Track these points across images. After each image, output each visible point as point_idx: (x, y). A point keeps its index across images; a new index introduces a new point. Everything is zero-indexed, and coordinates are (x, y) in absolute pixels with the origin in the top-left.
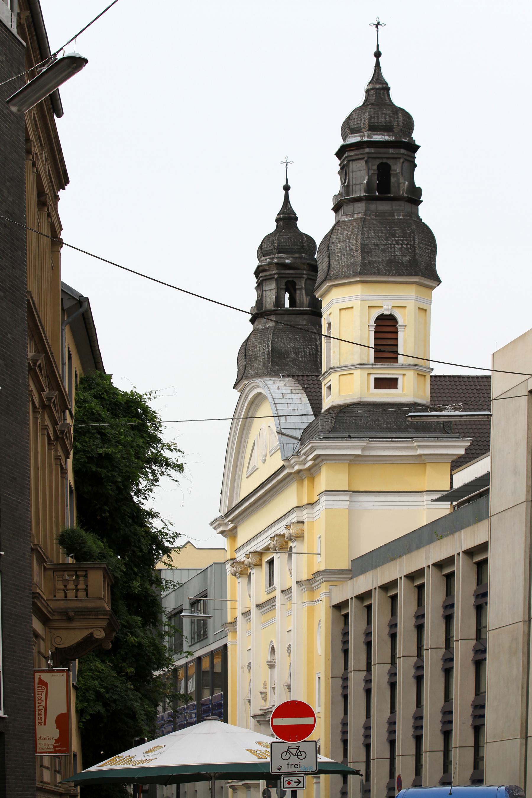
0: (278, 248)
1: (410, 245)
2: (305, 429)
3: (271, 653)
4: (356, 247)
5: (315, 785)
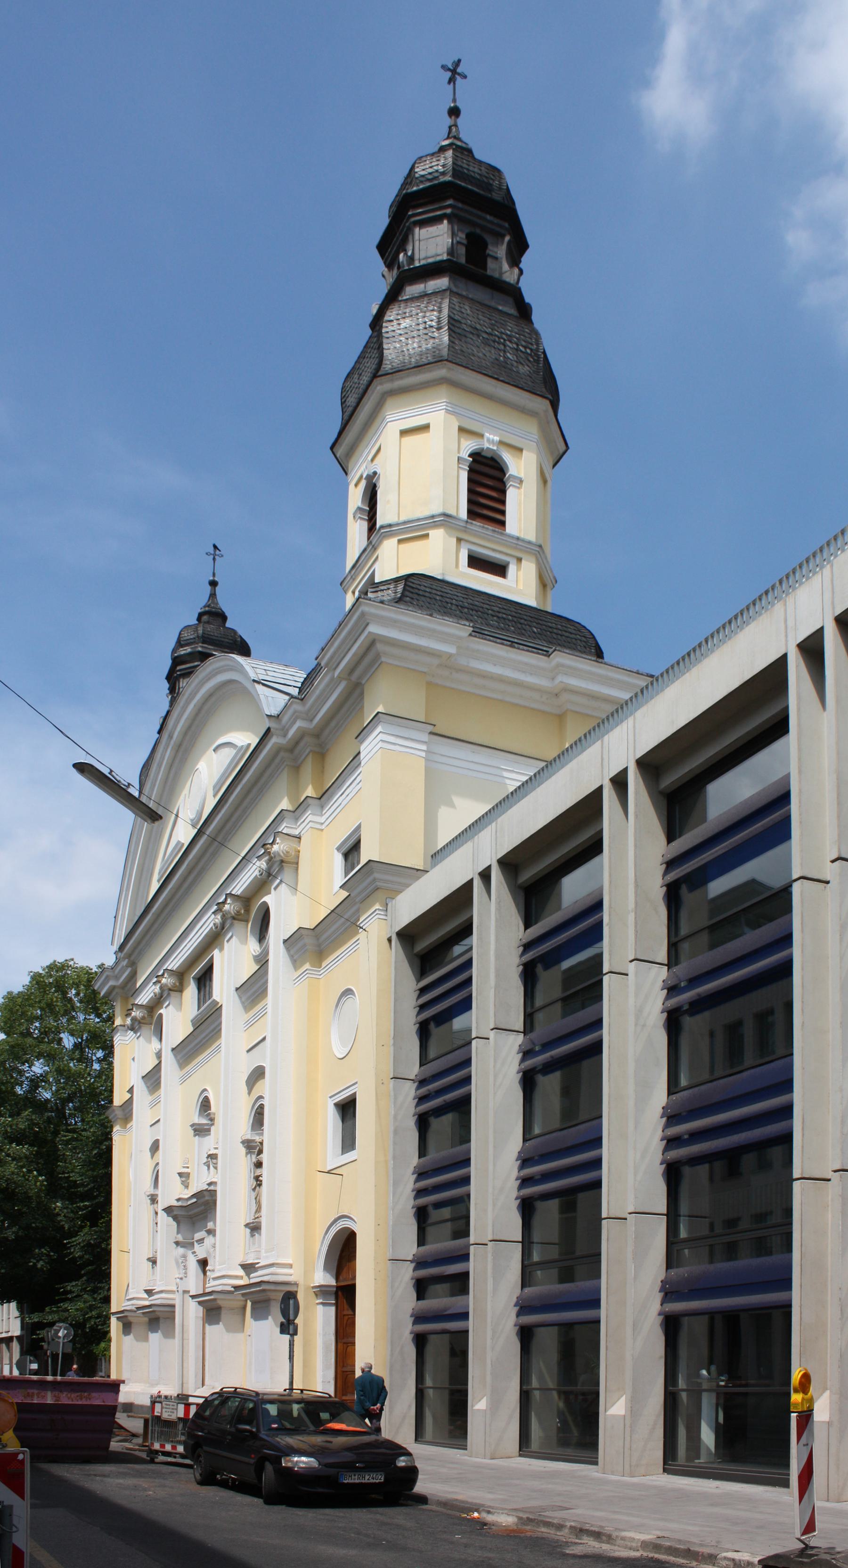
0: (203, 637)
1: (531, 350)
2: (300, 688)
3: (200, 1110)
4: (439, 321)
5: (321, 1307)
